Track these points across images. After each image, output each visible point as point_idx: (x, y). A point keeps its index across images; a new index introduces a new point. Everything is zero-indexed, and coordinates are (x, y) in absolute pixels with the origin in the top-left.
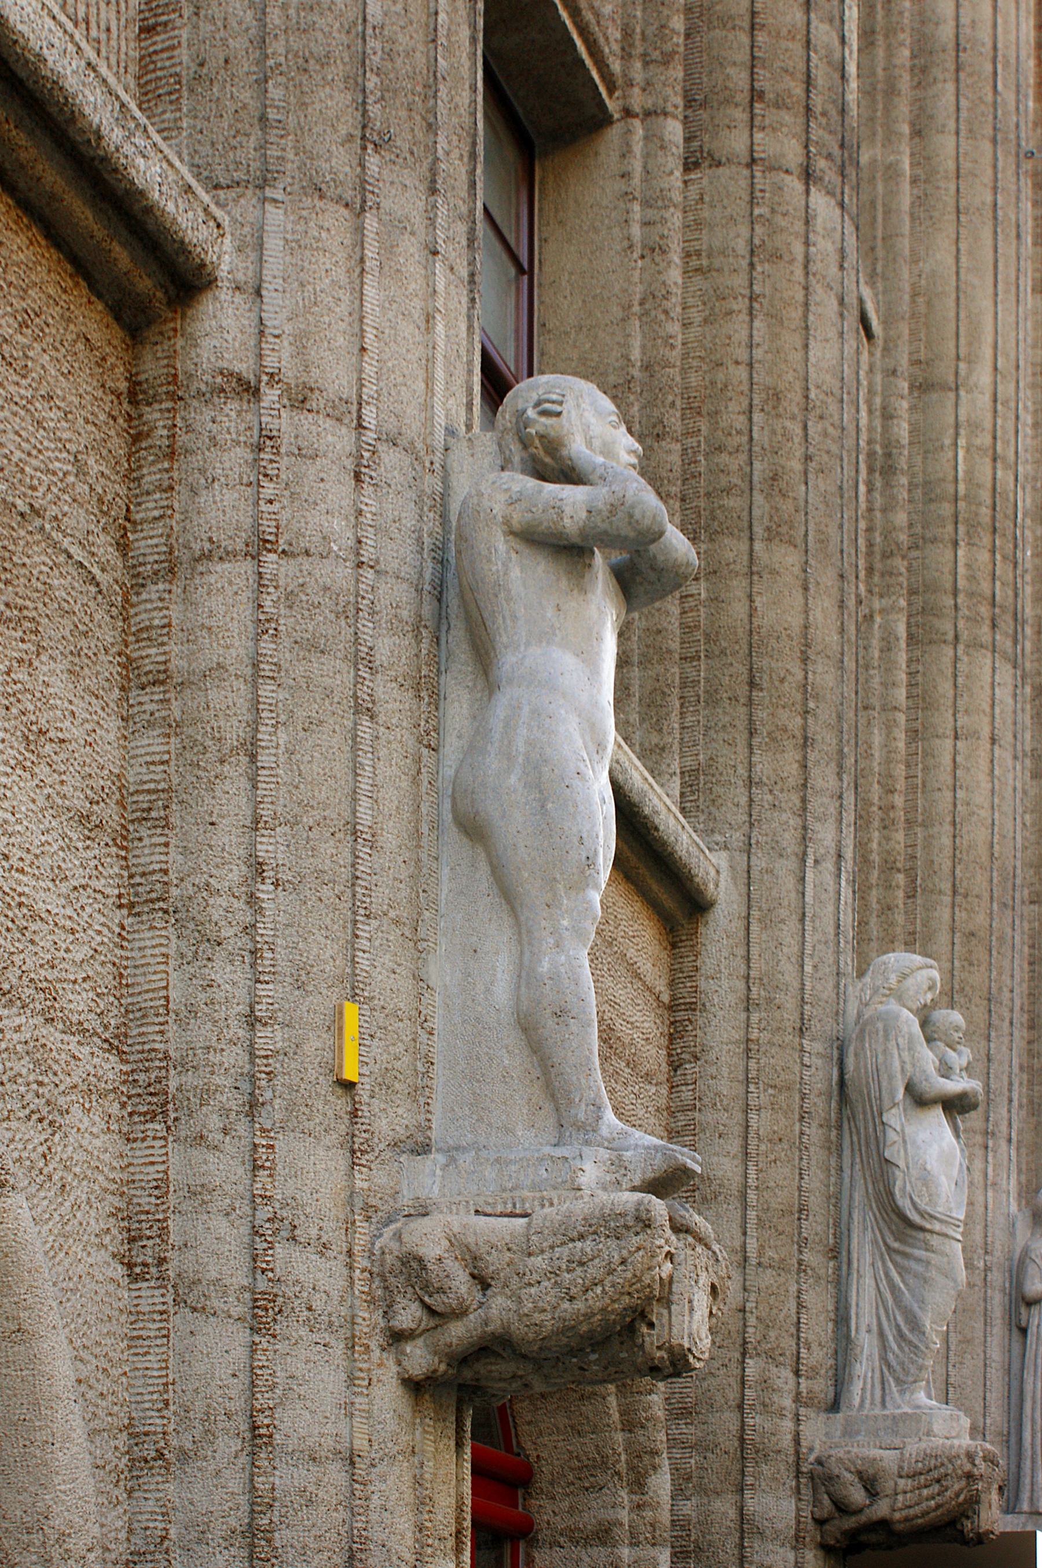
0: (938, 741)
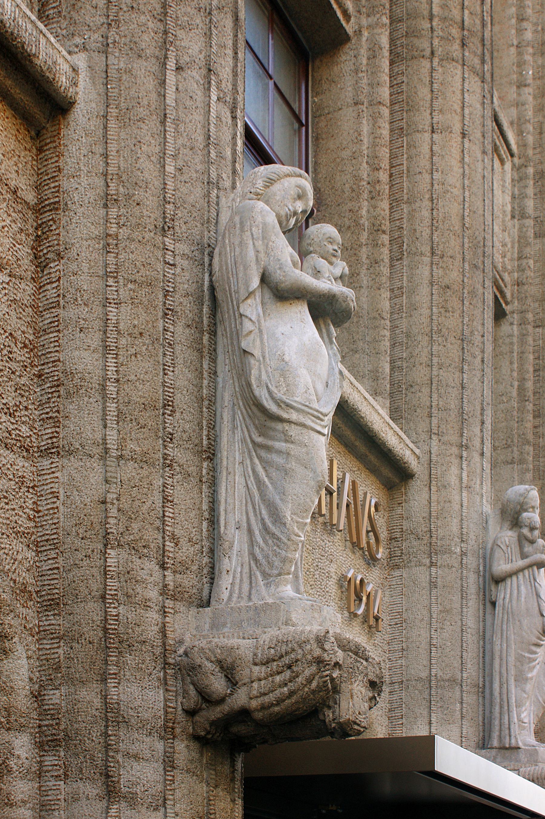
0: (419, 135)
